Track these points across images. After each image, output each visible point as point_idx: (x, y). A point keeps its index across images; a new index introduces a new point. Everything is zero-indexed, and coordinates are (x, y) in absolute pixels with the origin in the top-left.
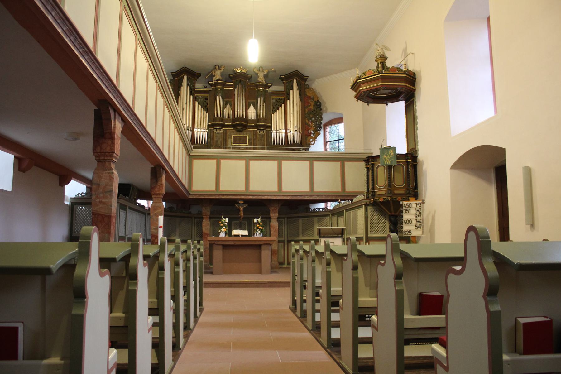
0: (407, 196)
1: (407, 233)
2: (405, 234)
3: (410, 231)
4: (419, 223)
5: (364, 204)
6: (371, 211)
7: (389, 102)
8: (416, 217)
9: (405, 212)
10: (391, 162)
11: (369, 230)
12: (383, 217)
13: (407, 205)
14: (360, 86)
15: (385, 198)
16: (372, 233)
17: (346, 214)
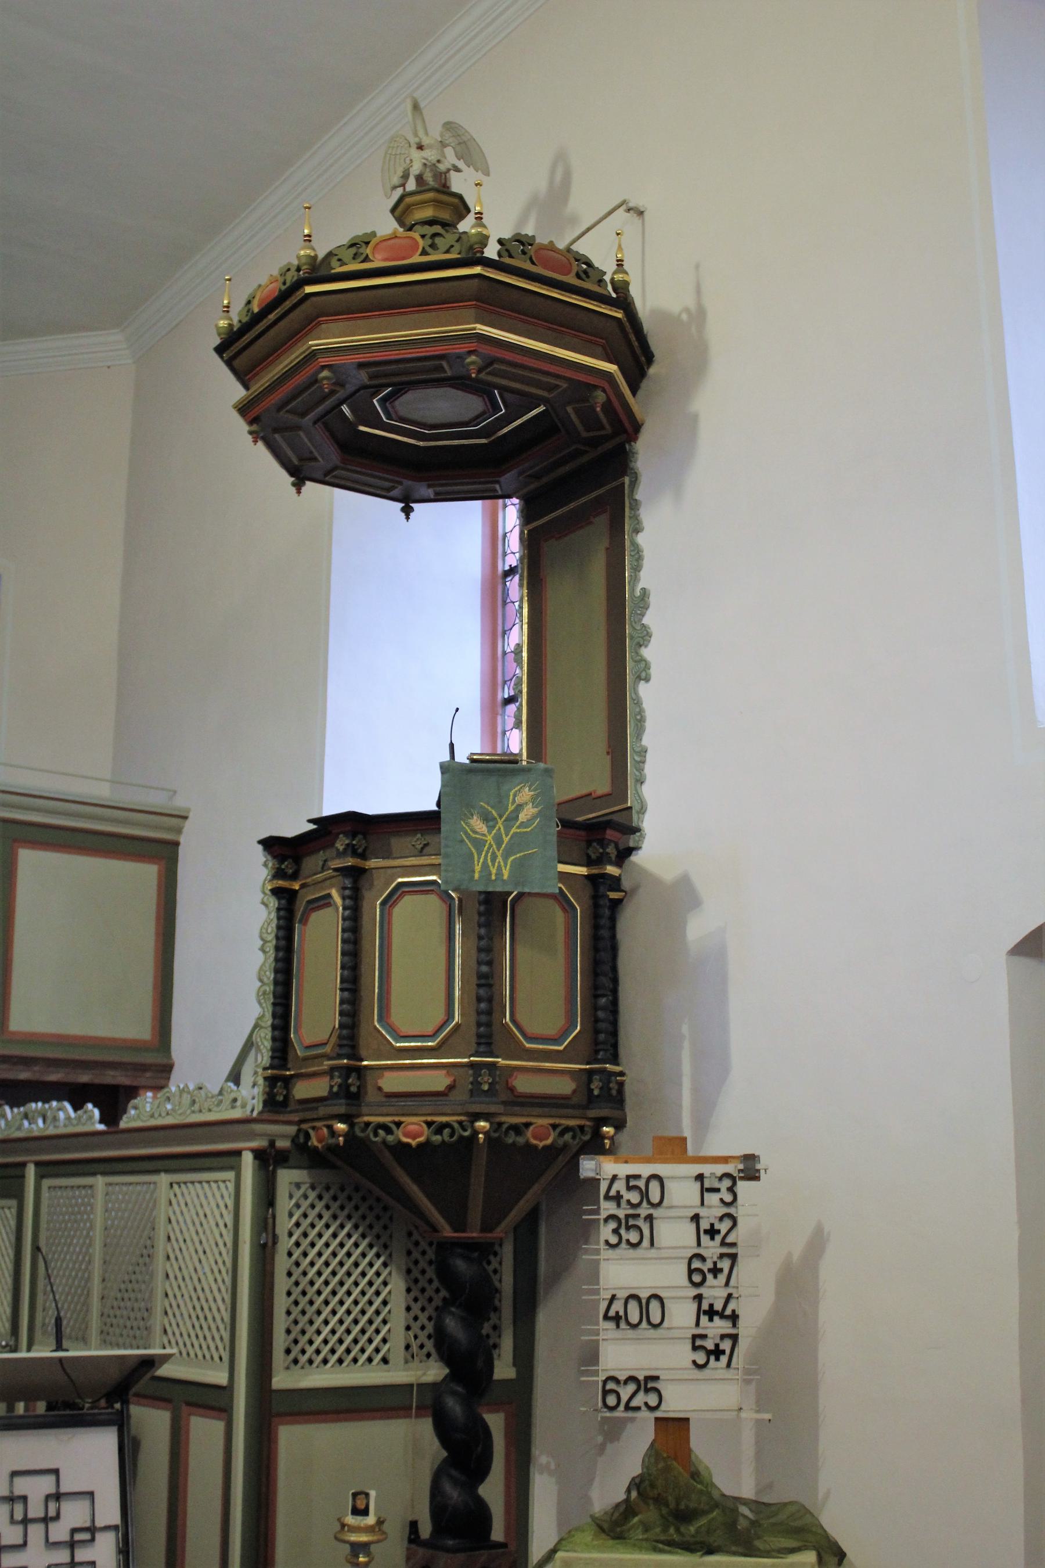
0: (593, 1113)
1: (626, 1392)
2: (611, 1400)
3: (648, 1379)
4: (719, 1326)
5: (253, 1150)
6: (298, 1206)
7: (430, 493)
8: (697, 1278)
9: (614, 1240)
10: (519, 867)
11: (280, 1340)
12: (371, 1246)
13: (629, 1188)
14: (309, 325)
15: (447, 1125)
16: (296, 1361)
17: (45, 1194)
